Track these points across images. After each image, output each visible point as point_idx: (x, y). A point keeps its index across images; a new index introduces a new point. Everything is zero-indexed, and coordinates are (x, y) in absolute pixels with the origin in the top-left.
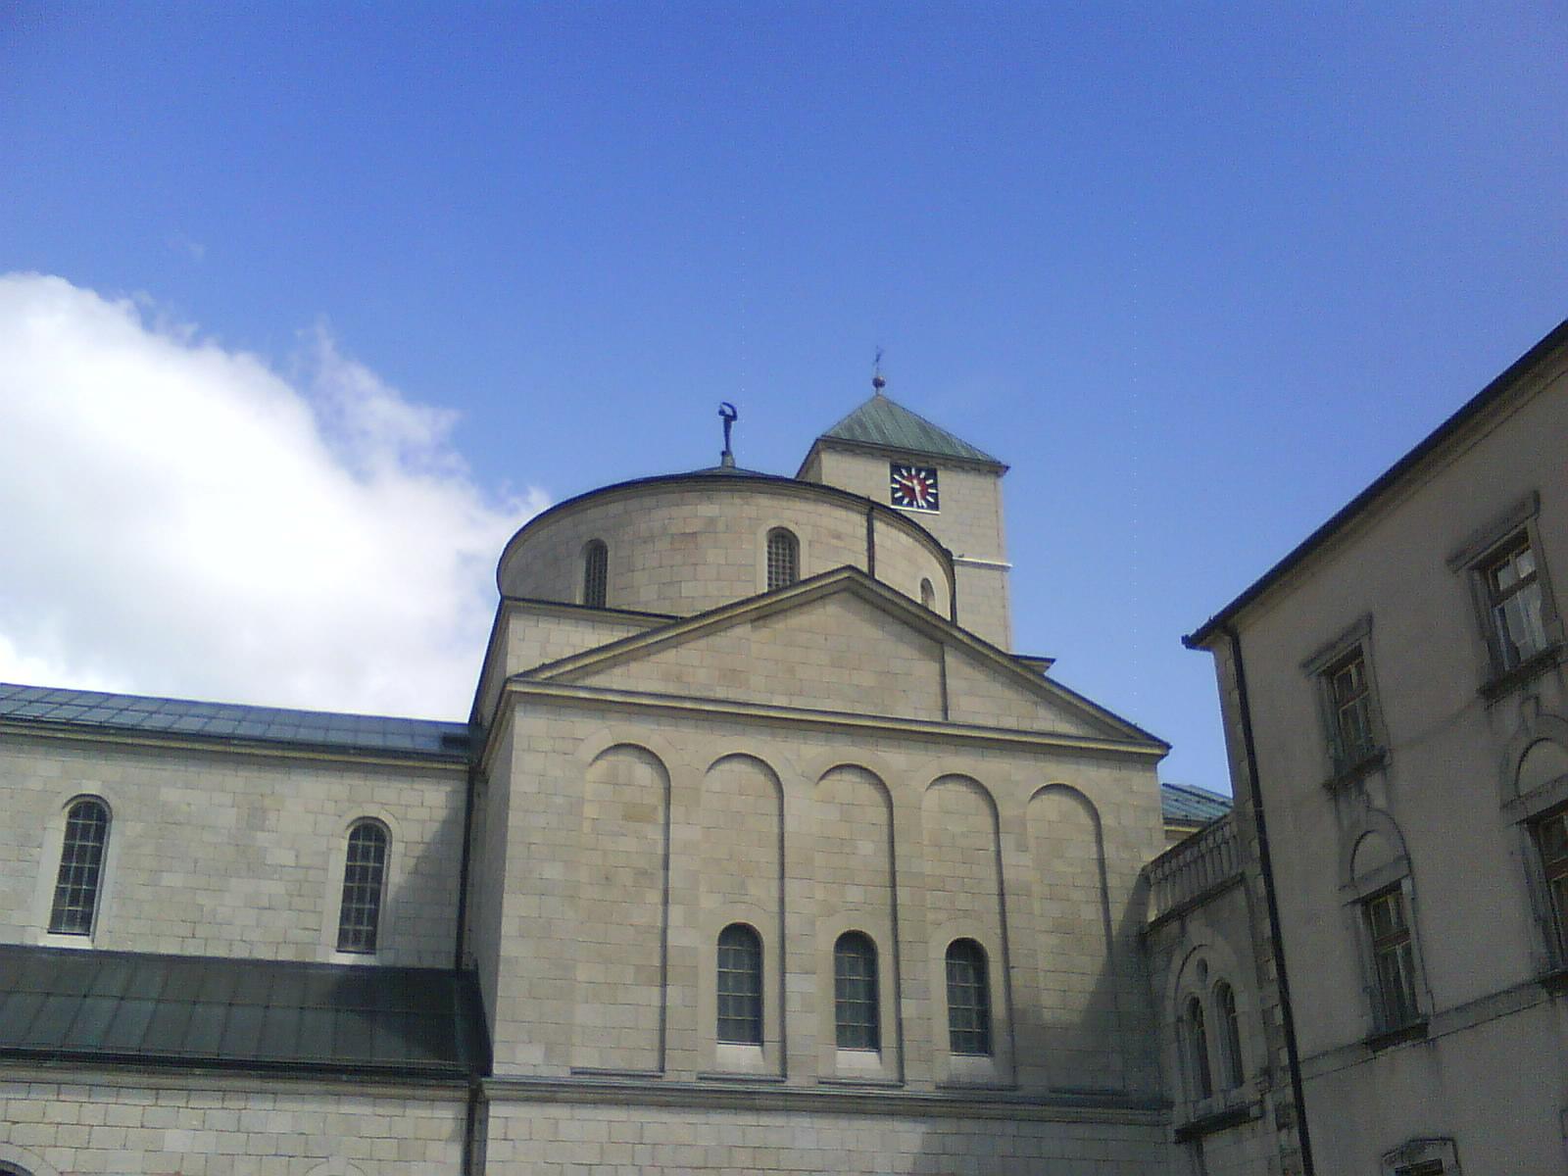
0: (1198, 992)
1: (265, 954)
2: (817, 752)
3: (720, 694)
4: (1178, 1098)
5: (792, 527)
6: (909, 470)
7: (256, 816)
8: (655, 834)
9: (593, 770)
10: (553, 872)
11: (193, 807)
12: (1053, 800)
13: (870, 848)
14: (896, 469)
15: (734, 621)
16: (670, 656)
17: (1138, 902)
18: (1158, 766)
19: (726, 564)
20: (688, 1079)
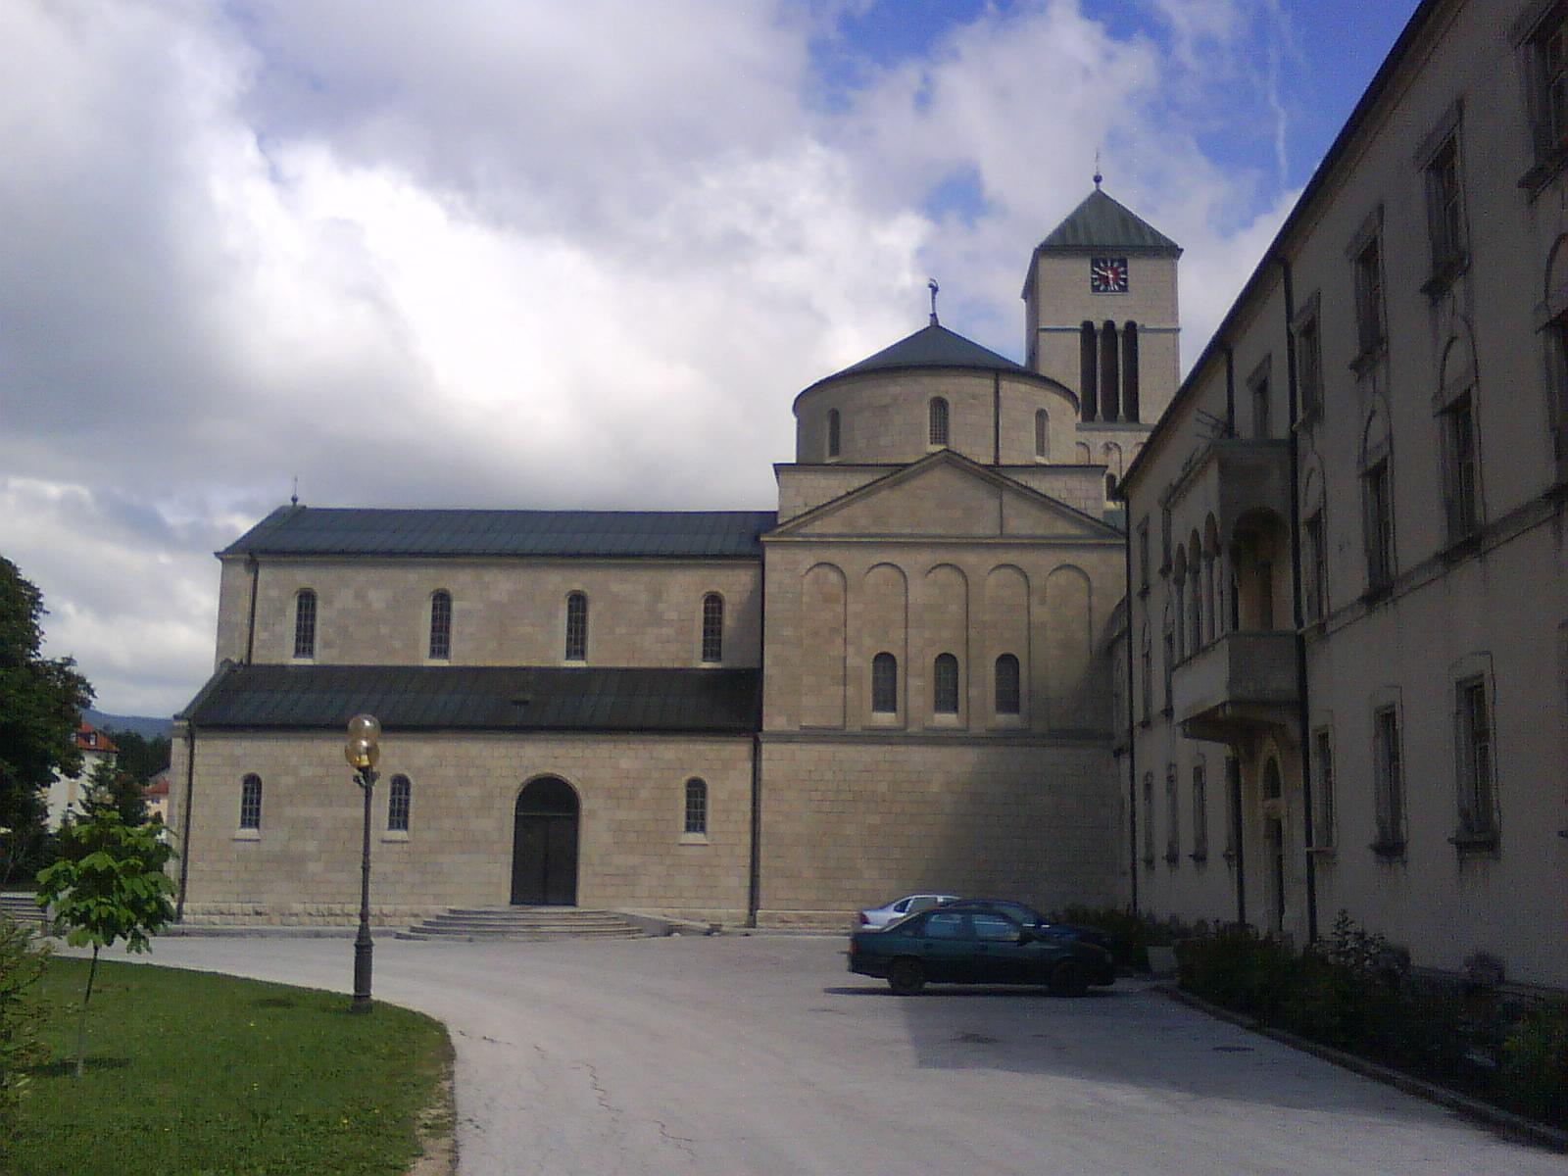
1: (669, 665)
2: (927, 557)
3: (873, 530)
6: (1105, 263)
7: (657, 595)
8: (839, 609)
9: (808, 577)
10: (788, 632)
13: (955, 609)
14: (1095, 263)
16: (845, 512)
20: (857, 729)
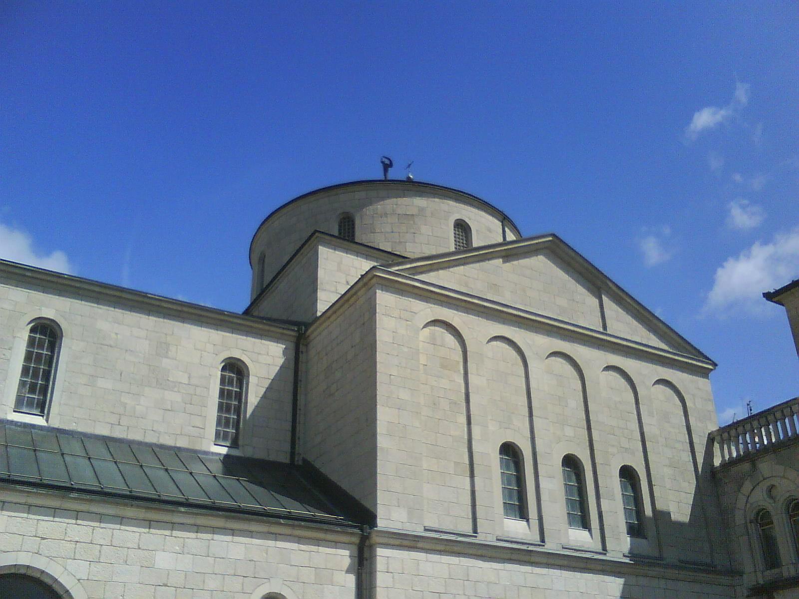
0: (768, 505)
4: (748, 568)
5: (467, 221)
7: (162, 348)
10: (404, 395)
11: (119, 336)
12: (661, 387)
15: (468, 260)
17: (709, 454)
18: (709, 375)
19: (432, 236)
20: (491, 540)
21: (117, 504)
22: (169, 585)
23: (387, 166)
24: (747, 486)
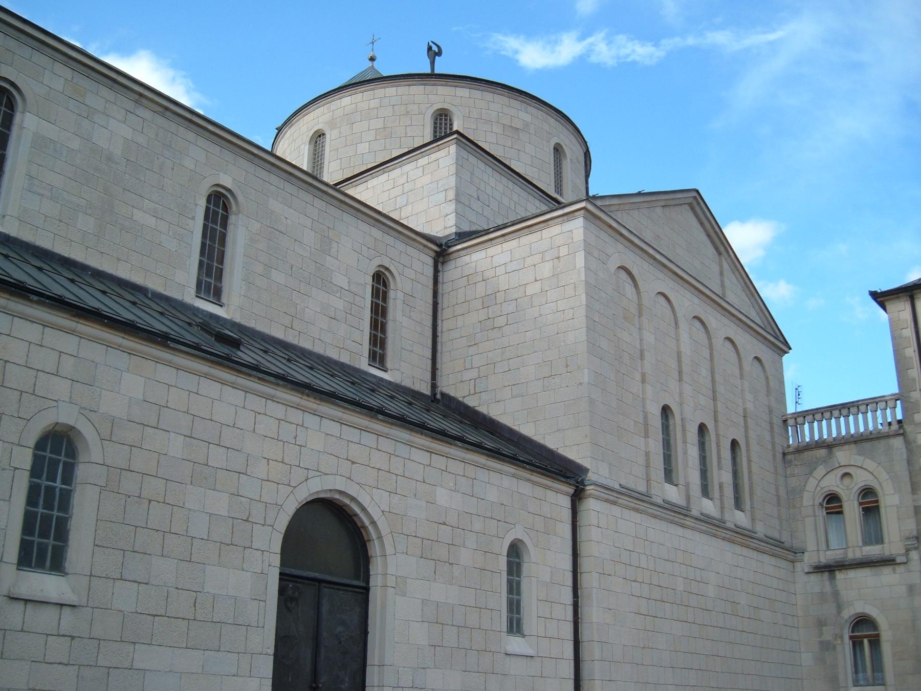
4: (811, 546)
21: (412, 430)
22: (447, 524)
23: (434, 53)
24: (821, 470)
